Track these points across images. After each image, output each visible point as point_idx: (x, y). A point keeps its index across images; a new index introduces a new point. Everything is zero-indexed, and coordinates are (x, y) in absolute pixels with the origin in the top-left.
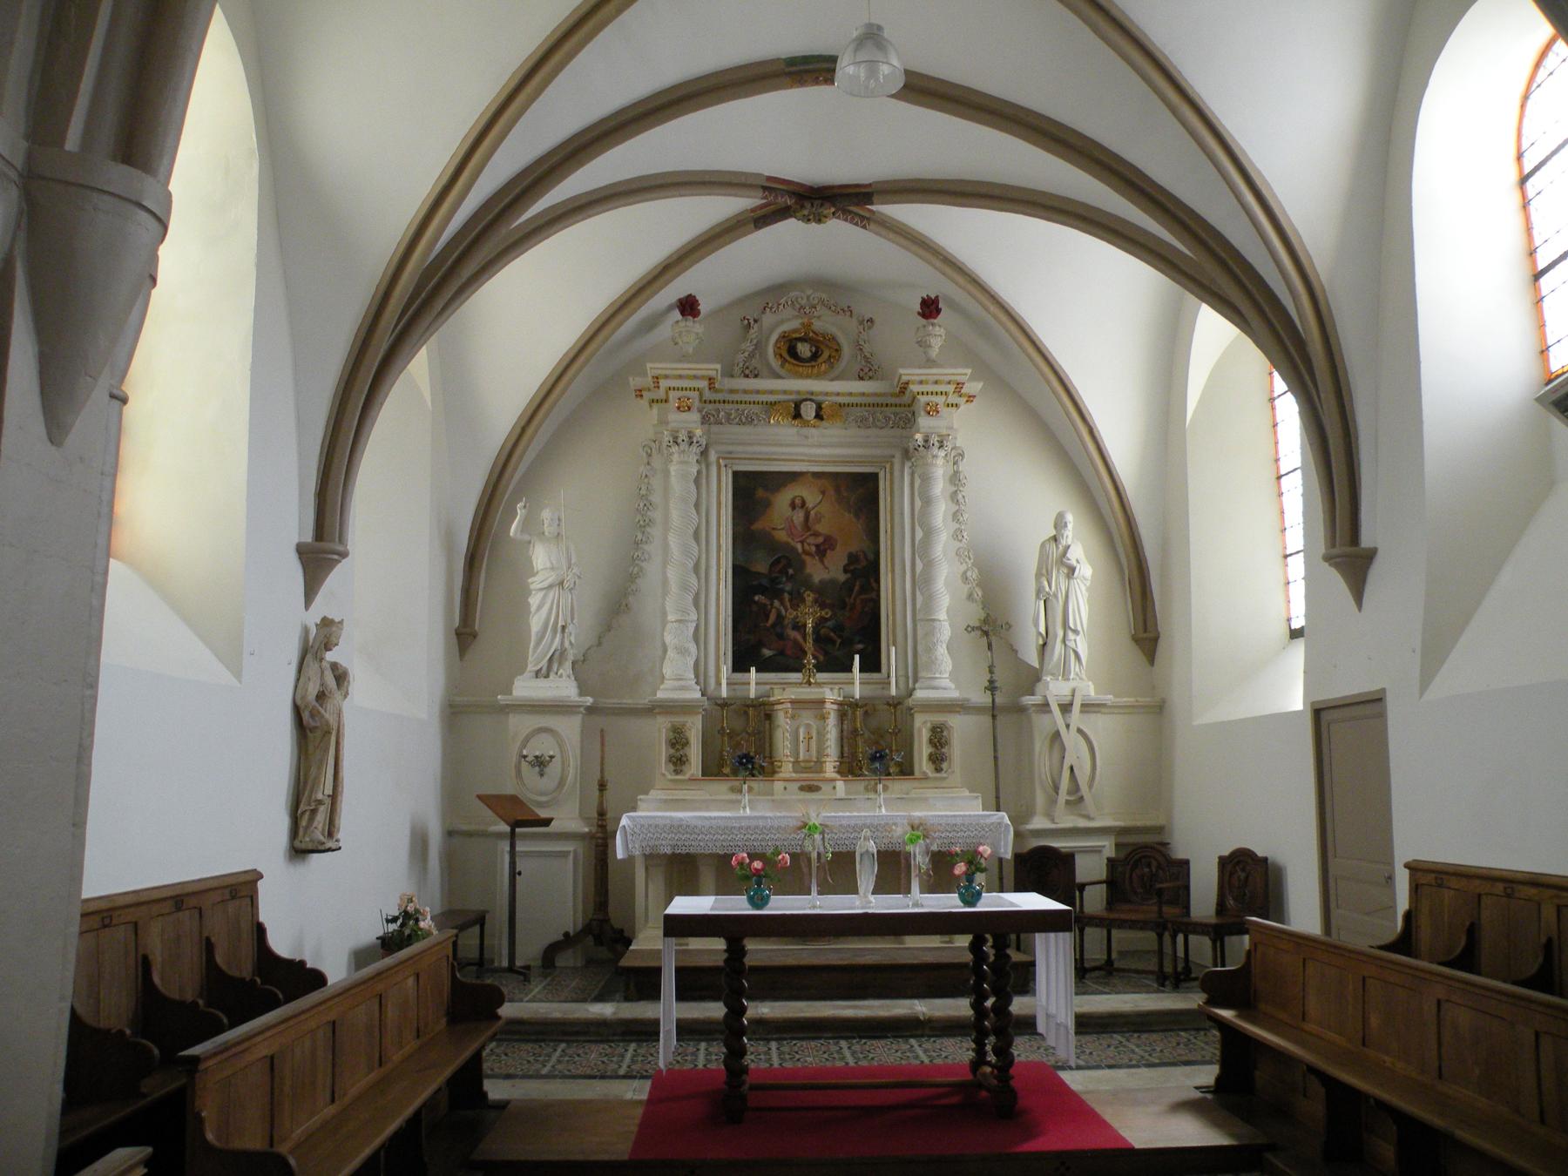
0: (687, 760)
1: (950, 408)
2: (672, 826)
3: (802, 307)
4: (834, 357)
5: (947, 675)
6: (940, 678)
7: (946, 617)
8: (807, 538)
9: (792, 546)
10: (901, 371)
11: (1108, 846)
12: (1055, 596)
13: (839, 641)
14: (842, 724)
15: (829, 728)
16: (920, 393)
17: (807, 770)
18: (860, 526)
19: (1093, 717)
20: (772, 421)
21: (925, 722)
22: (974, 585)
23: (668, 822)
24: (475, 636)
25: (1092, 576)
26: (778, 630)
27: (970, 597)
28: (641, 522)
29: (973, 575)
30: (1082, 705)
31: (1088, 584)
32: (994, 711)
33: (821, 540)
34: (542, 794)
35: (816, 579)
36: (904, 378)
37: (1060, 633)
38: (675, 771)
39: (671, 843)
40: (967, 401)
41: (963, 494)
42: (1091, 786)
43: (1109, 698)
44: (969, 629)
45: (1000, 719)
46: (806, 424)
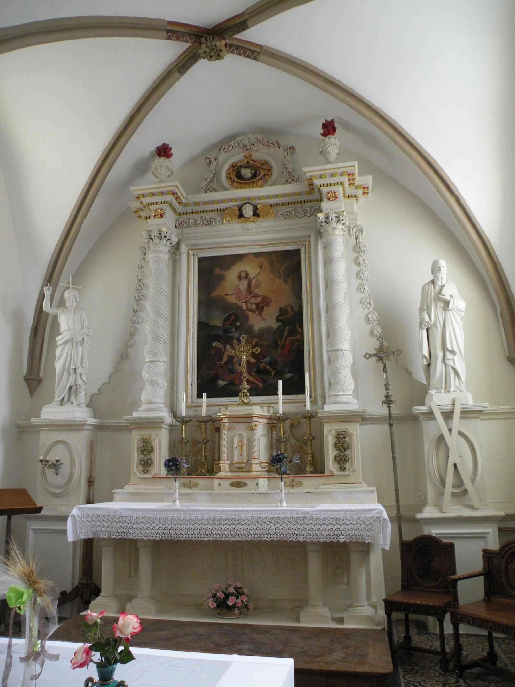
0: (152, 463)
1: (351, 199)
2: (109, 516)
3: (245, 146)
4: (267, 175)
5: (351, 393)
6: (344, 395)
7: (349, 348)
8: (250, 299)
9: (239, 306)
10: (305, 169)
11: (491, 534)
12: (435, 325)
13: (273, 372)
14: (272, 434)
15: (257, 436)
16: (322, 186)
17: (240, 470)
18: (287, 288)
19: (472, 422)
20: (224, 222)
21: (330, 431)
22: (375, 325)
23: (106, 513)
24: (40, 381)
25: (466, 308)
26: (230, 367)
27: (372, 333)
28: (137, 298)
29: (374, 316)
30: (462, 412)
31: (463, 314)
32: (390, 421)
33: (259, 300)
34: (58, 488)
35: (256, 328)
36: (308, 175)
37: (440, 354)
38: (143, 471)
39: (108, 529)
40: (364, 193)
41: (363, 258)
42: (473, 481)
43: (485, 405)
44: (367, 356)
45: (395, 426)
46: (248, 219)
